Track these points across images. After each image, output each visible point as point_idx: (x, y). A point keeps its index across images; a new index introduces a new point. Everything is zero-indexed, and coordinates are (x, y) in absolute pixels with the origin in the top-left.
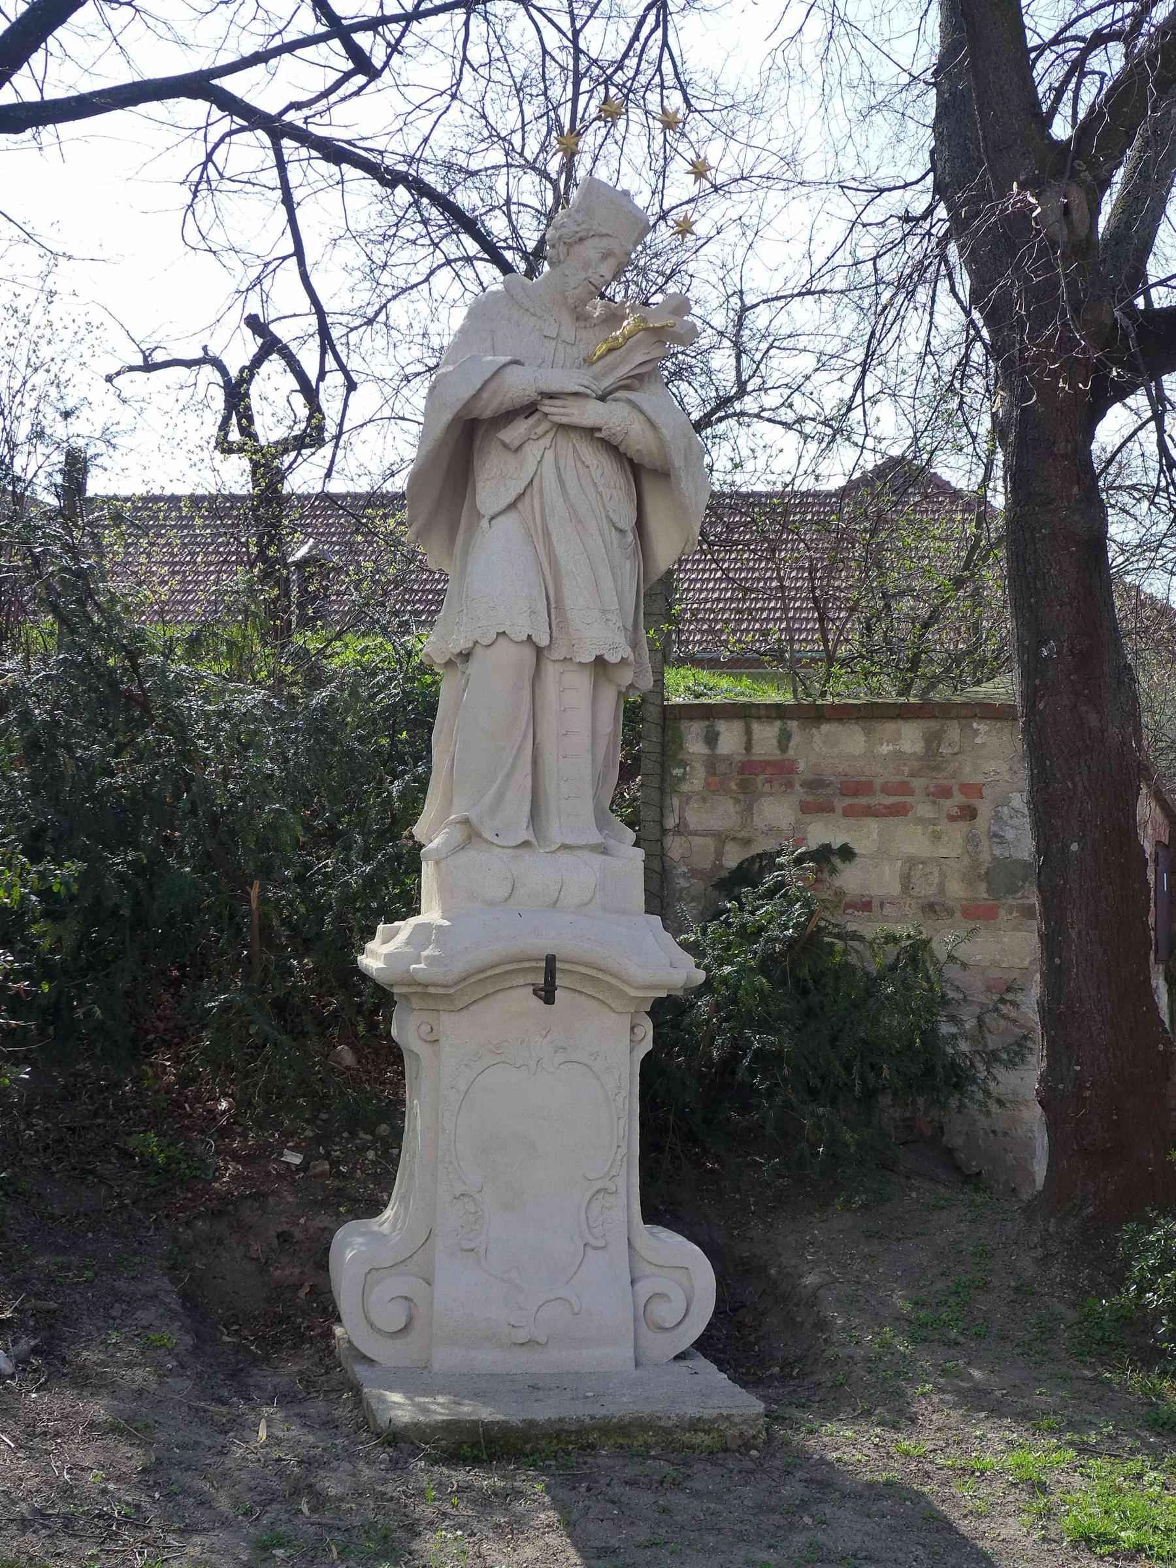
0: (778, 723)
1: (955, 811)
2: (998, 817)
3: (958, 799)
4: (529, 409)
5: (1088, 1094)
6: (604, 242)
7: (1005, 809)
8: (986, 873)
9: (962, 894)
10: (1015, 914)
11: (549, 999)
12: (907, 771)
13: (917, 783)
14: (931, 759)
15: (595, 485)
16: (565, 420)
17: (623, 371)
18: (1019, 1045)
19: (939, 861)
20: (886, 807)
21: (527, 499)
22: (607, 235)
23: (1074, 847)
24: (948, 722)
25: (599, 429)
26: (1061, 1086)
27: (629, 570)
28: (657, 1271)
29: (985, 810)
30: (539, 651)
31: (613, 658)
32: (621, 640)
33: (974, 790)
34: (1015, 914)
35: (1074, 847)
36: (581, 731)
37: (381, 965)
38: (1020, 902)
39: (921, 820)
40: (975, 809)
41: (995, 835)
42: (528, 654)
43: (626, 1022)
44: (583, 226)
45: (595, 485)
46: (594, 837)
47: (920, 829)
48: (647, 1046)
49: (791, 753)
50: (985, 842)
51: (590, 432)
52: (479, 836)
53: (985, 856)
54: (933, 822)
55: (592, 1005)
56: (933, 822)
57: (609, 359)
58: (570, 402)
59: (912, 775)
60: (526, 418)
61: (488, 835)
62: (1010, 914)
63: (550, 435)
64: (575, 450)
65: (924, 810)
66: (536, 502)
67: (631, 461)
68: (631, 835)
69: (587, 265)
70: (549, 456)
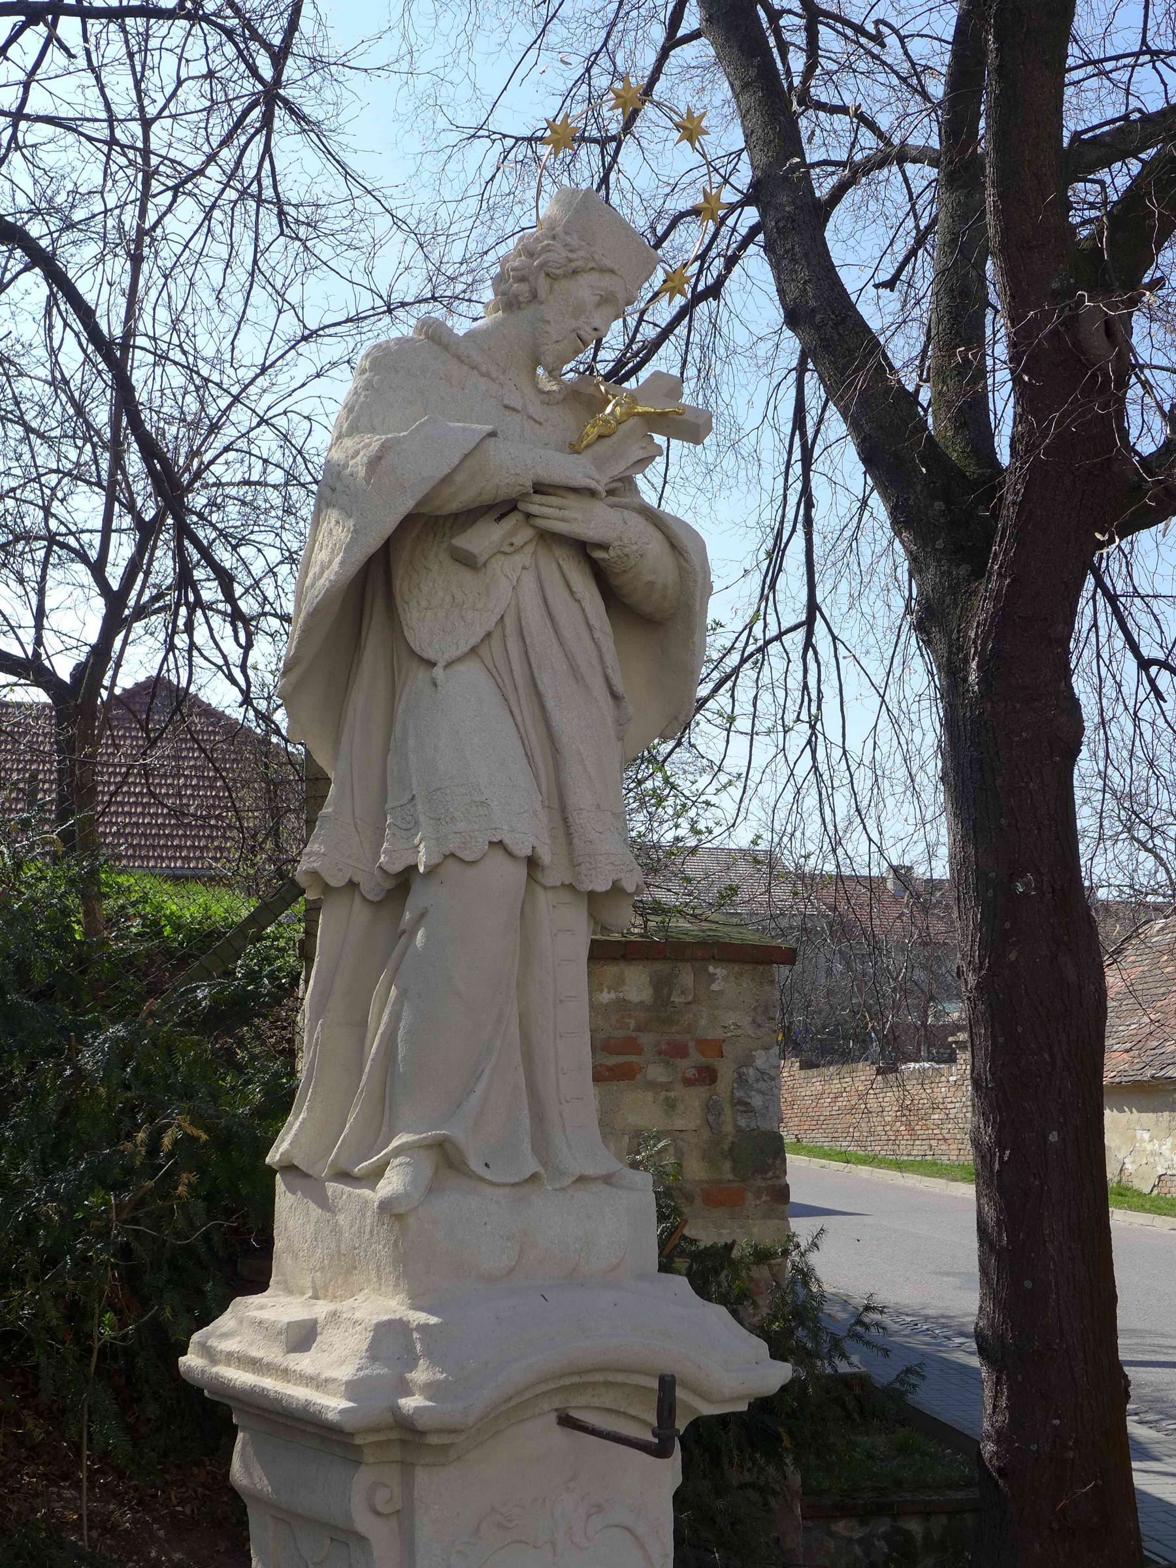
1: (691, 1073)
2: (741, 1079)
3: (695, 1058)
4: (505, 508)
5: (1071, 1454)
6: (607, 281)
7: (751, 1071)
8: (731, 1149)
9: (703, 1175)
10: (764, 1198)
12: (632, 1023)
13: (646, 1039)
14: (662, 1008)
15: (590, 627)
18: (902, 1382)
19: (674, 1134)
20: (609, 1069)
22: (612, 271)
23: (1053, 1137)
24: (680, 965)
26: (1034, 1447)
29: (726, 1072)
33: (716, 1048)
34: (764, 1198)
35: (1053, 1137)
37: (345, 1404)
38: (770, 1183)
39: (652, 1085)
40: (714, 1071)
41: (740, 1102)
44: (581, 253)
45: (590, 627)
47: (650, 1096)
50: (728, 1111)
51: (583, 549)
53: (728, 1128)
54: (667, 1087)
56: (667, 1087)
58: (571, 500)
59: (639, 1029)
60: (498, 519)
61: (475, 1165)
62: (759, 1198)
63: (530, 548)
65: (656, 1072)
69: (579, 311)
70: (529, 583)
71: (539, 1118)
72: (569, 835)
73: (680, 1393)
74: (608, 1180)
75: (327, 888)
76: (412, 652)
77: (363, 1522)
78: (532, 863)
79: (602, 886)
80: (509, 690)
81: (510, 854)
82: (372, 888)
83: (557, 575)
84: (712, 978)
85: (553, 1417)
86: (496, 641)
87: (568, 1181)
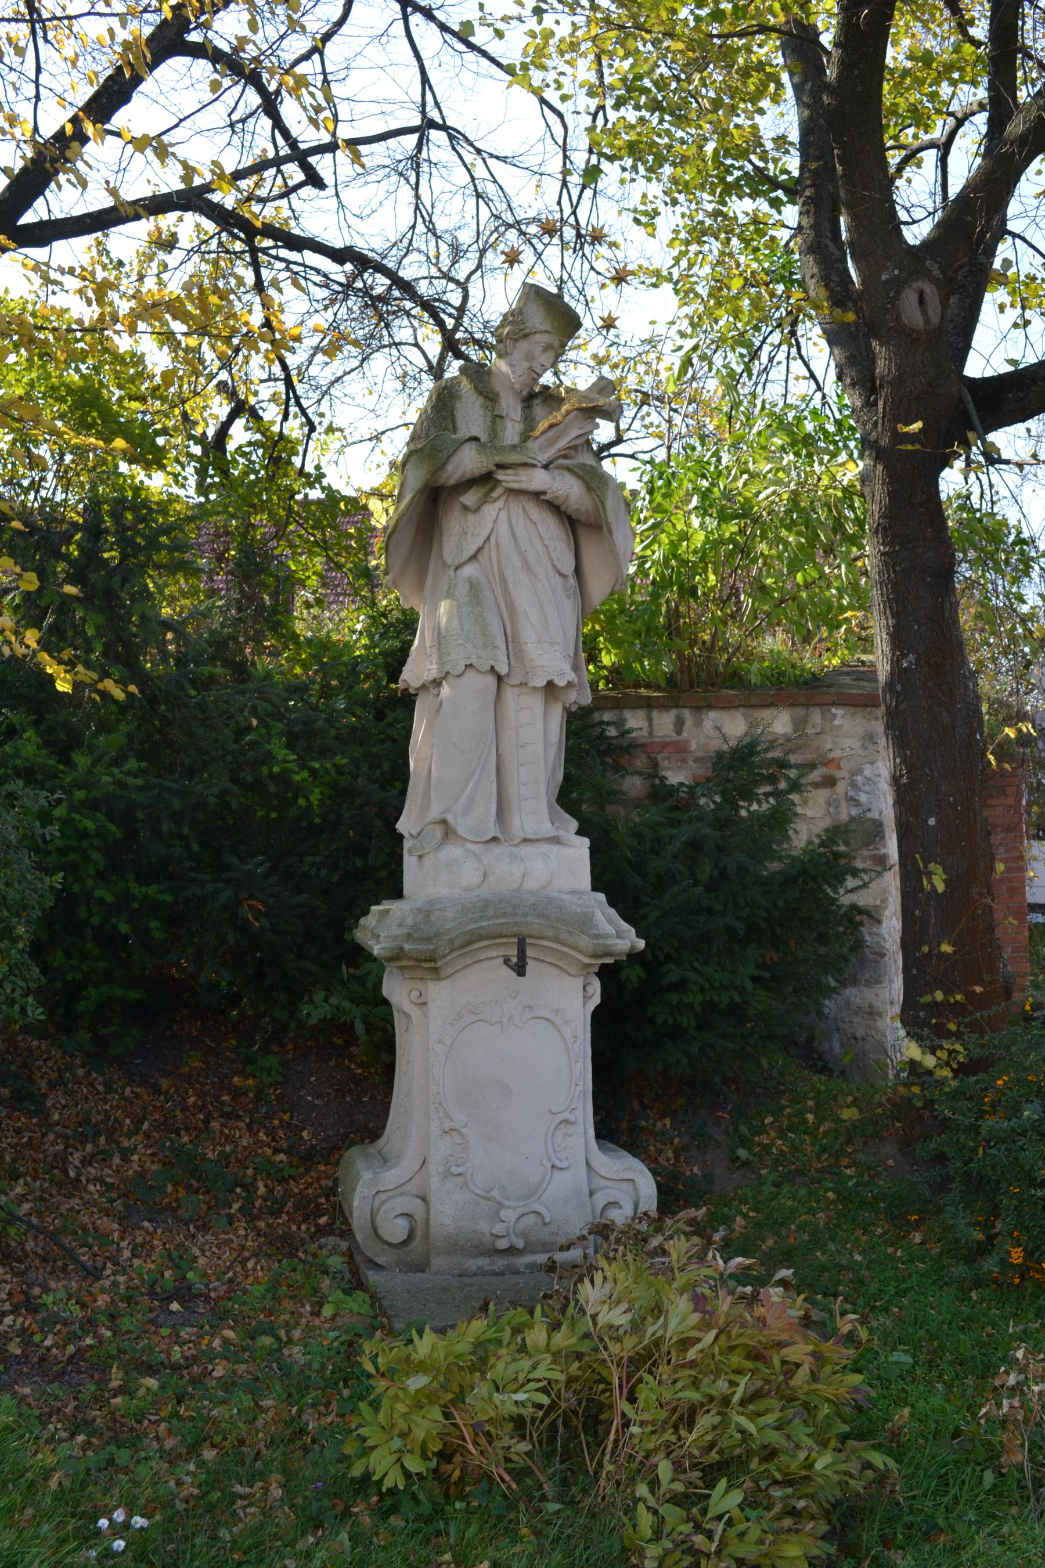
0: (674, 712)
2: (854, 785)
7: (859, 778)
11: (520, 970)
15: (542, 539)
16: (515, 486)
17: (562, 443)
21: (486, 550)
25: (544, 493)
27: (570, 609)
28: (610, 1184)
30: (500, 678)
31: (561, 683)
32: (567, 667)
36: (537, 742)
41: (852, 799)
42: (491, 681)
43: (579, 982)
45: (542, 539)
46: (548, 829)
48: (597, 1000)
49: (685, 734)
51: (537, 495)
52: (455, 833)
55: (554, 971)
57: (551, 433)
61: (461, 831)
64: (524, 510)
66: (494, 554)
67: (569, 518)
68: (574, 825)
70: (503, 515)
84: (834, 716)
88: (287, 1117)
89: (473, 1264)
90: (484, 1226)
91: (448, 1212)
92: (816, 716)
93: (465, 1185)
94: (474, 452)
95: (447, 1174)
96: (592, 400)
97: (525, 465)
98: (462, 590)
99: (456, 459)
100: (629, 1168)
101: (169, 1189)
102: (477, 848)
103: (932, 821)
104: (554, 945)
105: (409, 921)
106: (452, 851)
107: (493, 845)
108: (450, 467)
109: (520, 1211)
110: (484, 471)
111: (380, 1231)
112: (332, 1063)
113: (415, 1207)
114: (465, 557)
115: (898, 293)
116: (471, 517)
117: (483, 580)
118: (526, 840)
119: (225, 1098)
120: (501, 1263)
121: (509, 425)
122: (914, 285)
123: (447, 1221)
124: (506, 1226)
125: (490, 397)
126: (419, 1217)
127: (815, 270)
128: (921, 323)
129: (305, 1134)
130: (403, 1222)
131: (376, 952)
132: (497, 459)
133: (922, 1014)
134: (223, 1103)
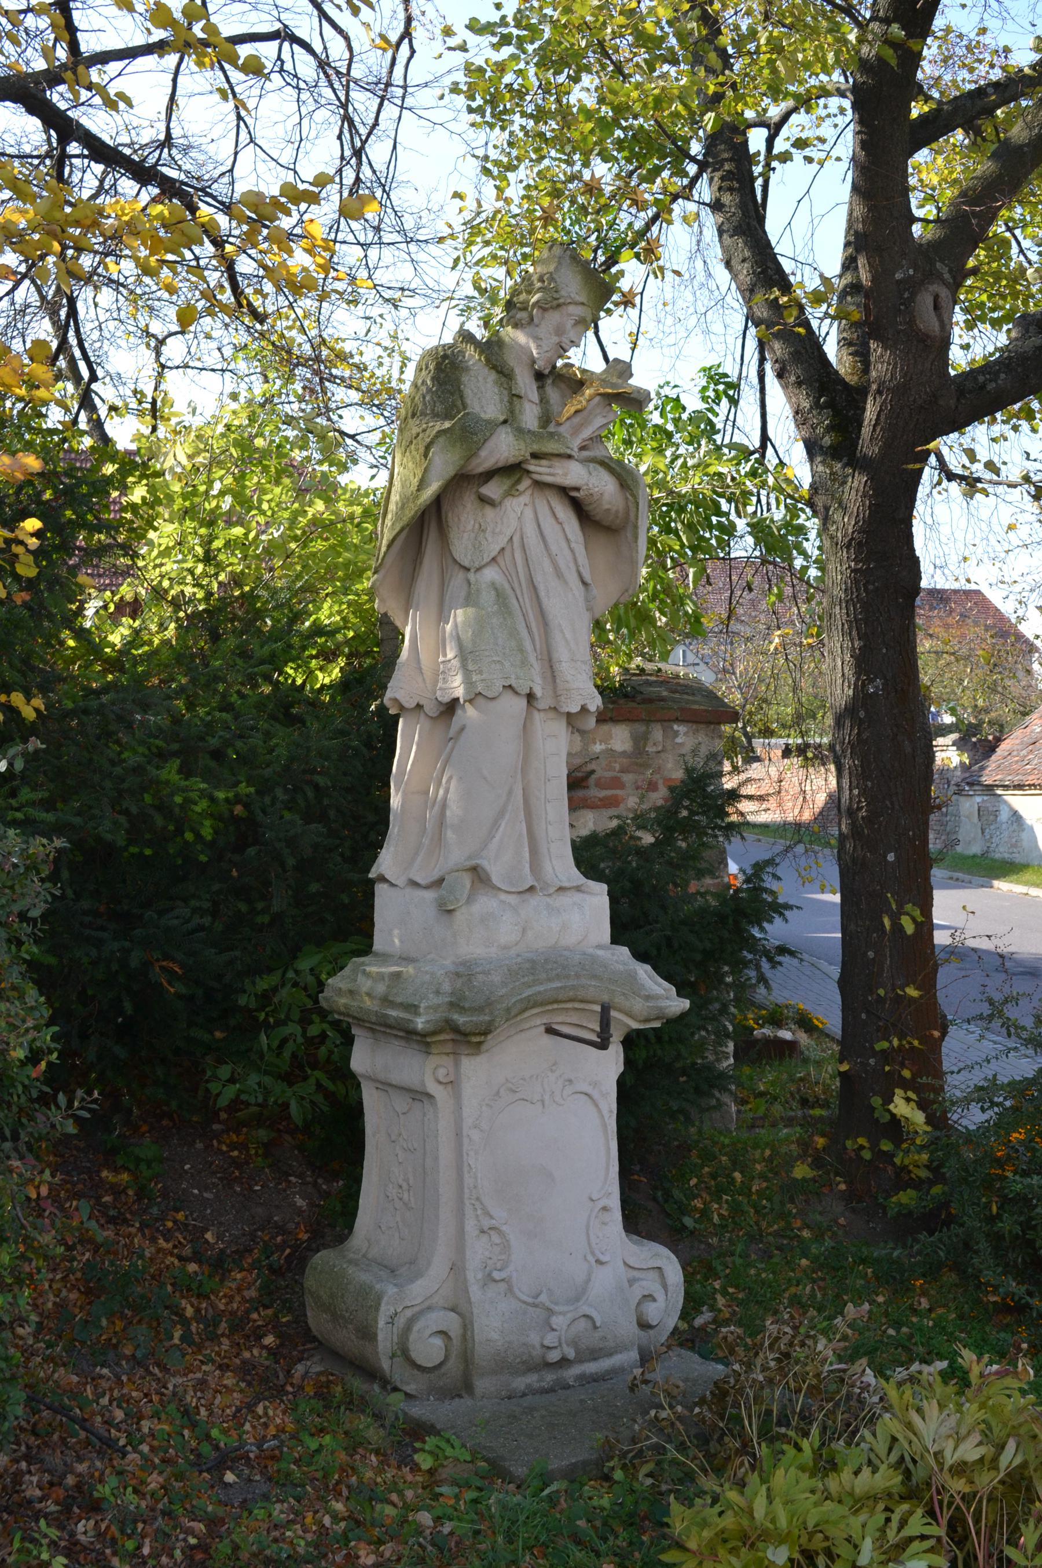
12: (617, 767)
15: (568, 540)
45: (568, 540)
51: (563, 491)
57: (576, 420)
61: (495, 880)
66: (518, 555)
70: (529, 513)
71: (534, 851)
72: (554, 677)
73: (613, 1013)
74: (578, 889)
75: (402, 708)
76: (455, 561)
77: (432, 1088)
78: (530, 697)
79: (575, 709)
80: (516, 586)
81: (516, 693)
82: (430, 709)
83: (547, 508)
84: (676, 734)
85: (542, 1029)
86: (508, 553)
87: (552, 890)
88: (180, 1216)
89: (521, 1383)
90: (534, 1339)
91: (495, 1325)
92: (657, 733)
93: (510, 1290)
94: (511, 438)
95: (489, 1279)
96: (613, 386)
97: (559, 456)
98: (487, 598)
99: (490, 444)
100: (657, 1255)
101: (104, 1322)
102: (512, 899)
103: (891, 857)
104: (577, 1005)
105: (447, 987)
106: (485, 903)
107: (527, 896)
108: (483, 453)
109: (570, 1316)
110: (512, 460)
111: (413, 1355)
112: (199, 1145)
113: (451, 1322)
114: (486, 560)
115: (913, 295)
116: (489, 511)
117: (507, 586)
118: (561, 889)
119: (107, 1199)
120: (549, 1377)
121: (527, 406)
122: (931, 288)
123: (495, 1336)
124: (561, 1333)
125: (504, 373)
126: (455, 1332)
127: (747, 254)
128: (937, 328)
129: (209, 1236)
130: (438, 1341)
131: (420, 1026)
132: (535, 447)
133: (872, 1061)
134: (105, 1206)
